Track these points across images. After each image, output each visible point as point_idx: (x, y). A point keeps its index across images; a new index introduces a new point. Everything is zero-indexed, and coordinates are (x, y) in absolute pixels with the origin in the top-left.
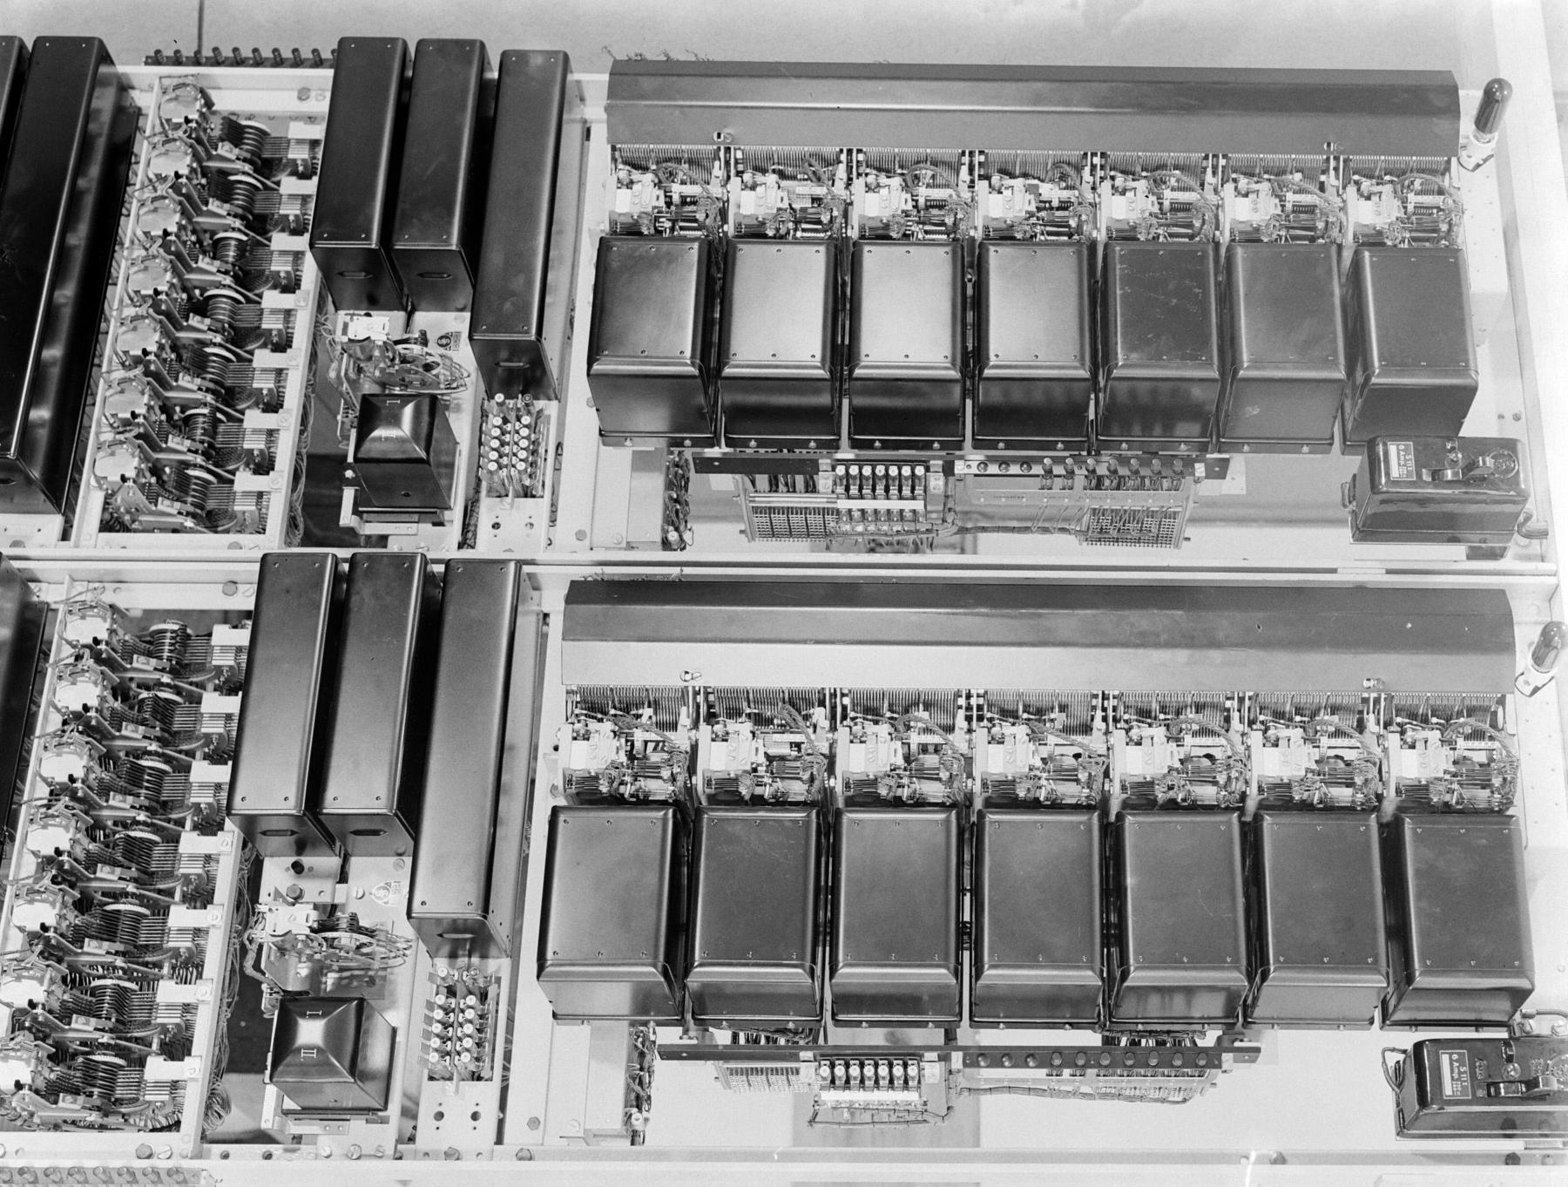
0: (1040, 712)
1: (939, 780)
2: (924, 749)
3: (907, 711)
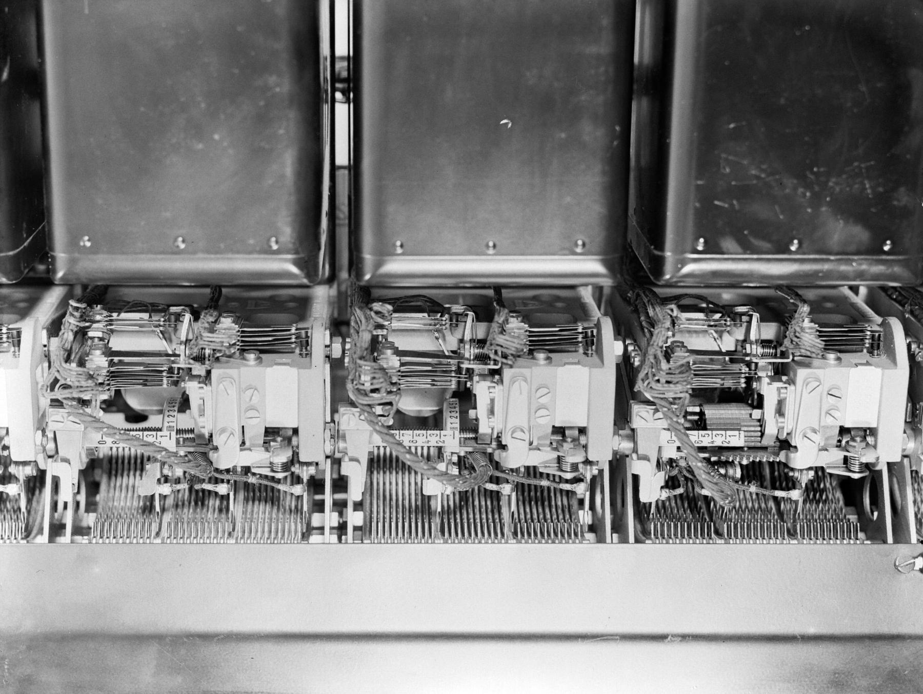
0: (200, 498)
1: (399, 353)
2: (434, 422)
3: (464, 497)
